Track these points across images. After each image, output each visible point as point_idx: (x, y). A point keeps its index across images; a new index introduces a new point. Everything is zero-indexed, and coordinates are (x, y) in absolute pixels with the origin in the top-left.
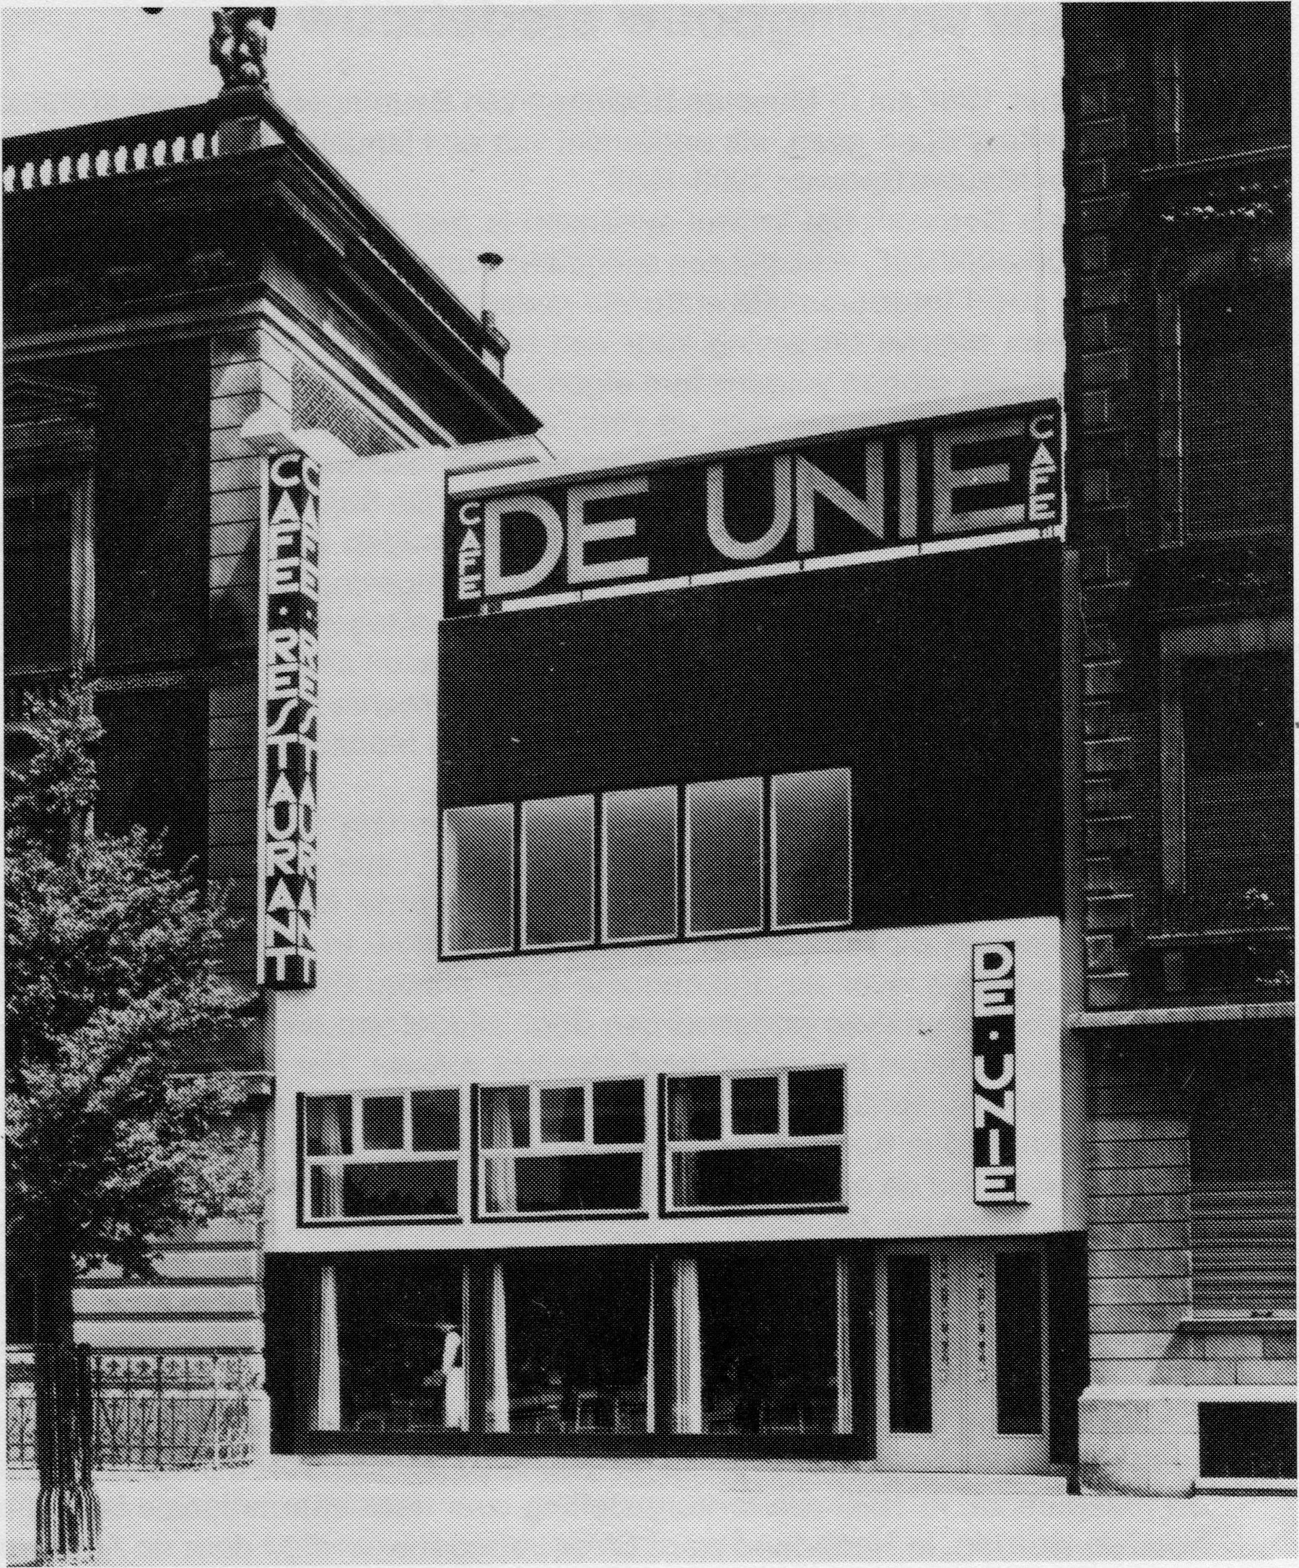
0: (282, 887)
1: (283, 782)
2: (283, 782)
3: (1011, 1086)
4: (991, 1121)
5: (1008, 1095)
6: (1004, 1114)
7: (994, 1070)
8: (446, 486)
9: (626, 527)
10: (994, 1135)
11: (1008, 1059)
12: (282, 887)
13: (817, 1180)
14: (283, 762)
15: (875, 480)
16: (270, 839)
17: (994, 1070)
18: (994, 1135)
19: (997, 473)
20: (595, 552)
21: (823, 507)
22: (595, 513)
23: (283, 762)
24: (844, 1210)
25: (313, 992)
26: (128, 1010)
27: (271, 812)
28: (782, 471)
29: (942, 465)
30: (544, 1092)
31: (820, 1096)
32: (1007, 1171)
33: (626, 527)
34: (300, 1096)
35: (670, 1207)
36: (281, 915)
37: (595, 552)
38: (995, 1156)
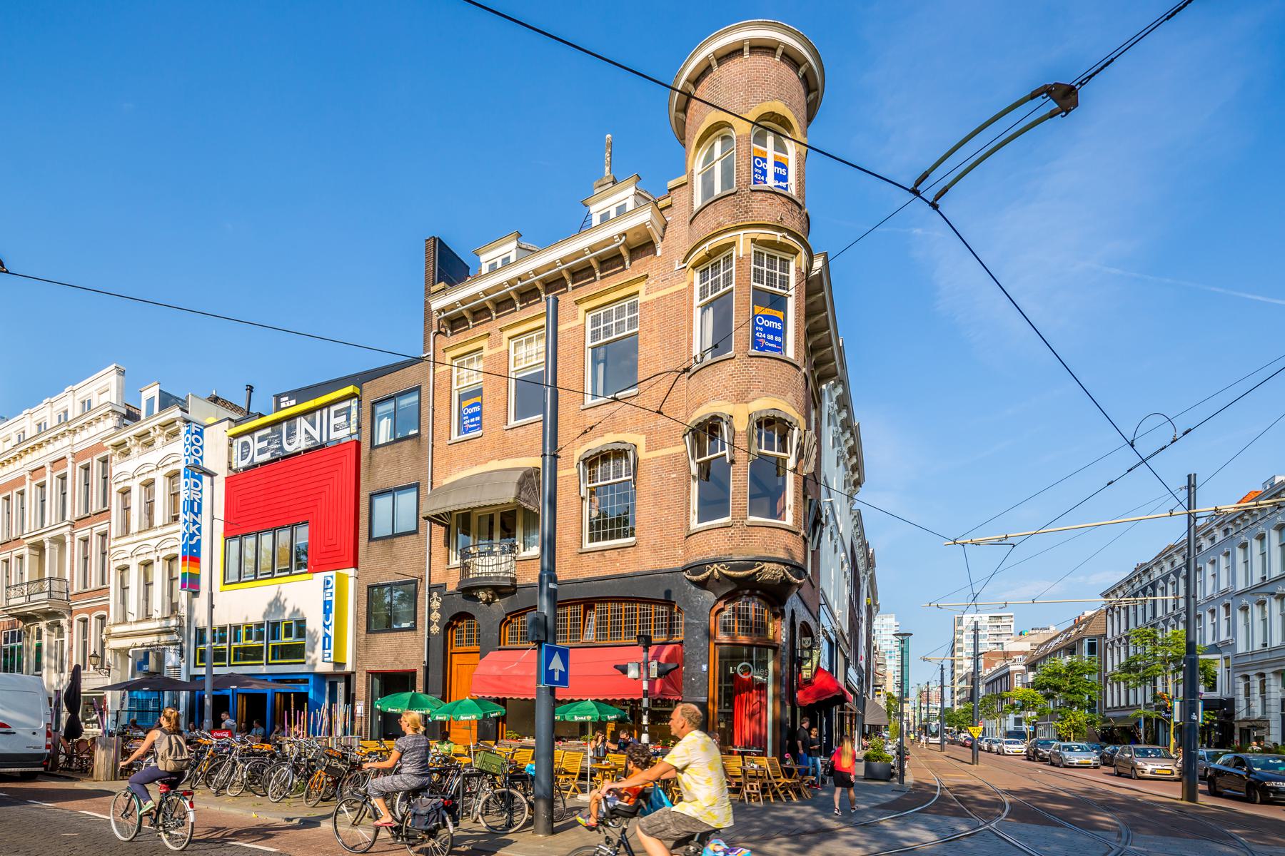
22: (261, 439)
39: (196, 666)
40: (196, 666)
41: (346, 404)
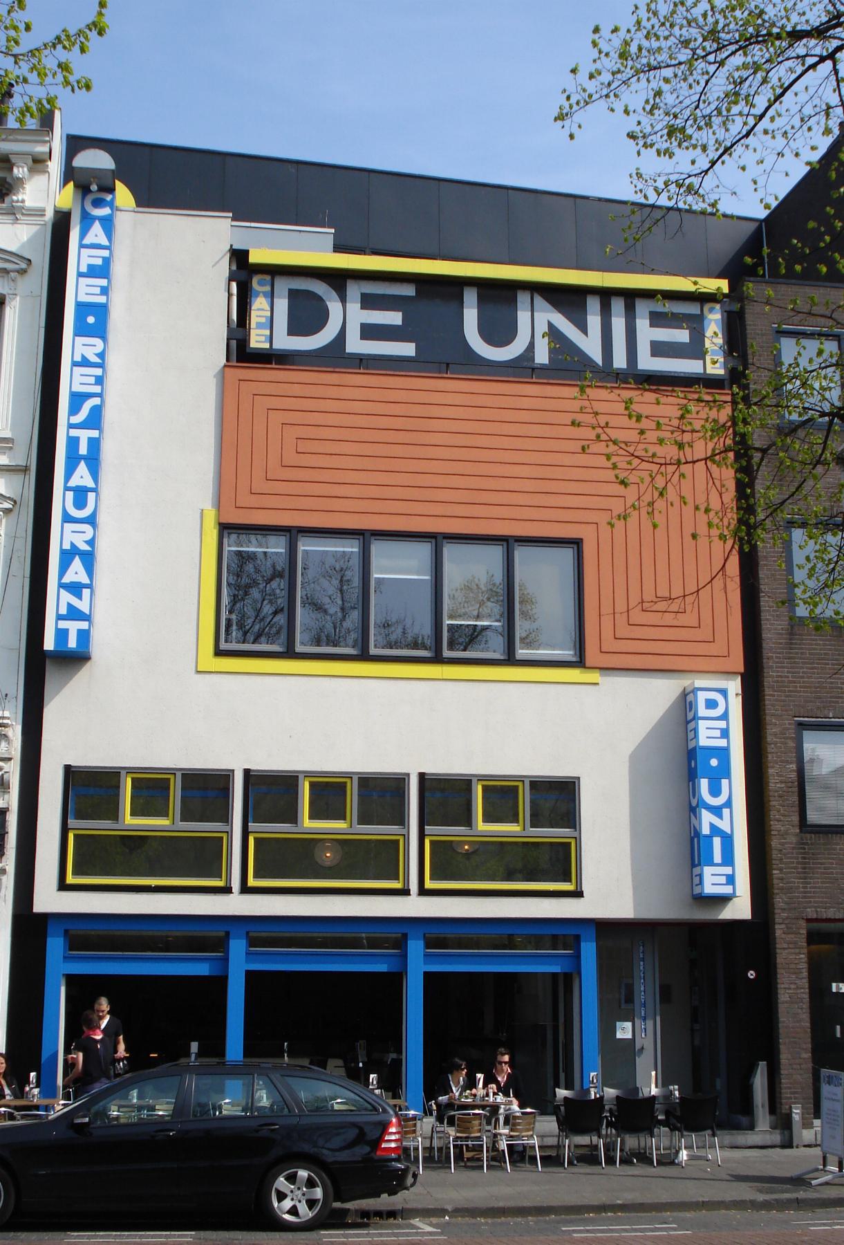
0: (77, 564)
1: (82, 468)
2: (82, 468)
3: (728, 804)
4: (715, 830)
5: (726, 812)
6: (724, 825)
7: (715, 791)
8: (109, 282)
9: (394, 318)
10: (717, 842)
11: (725, 782)
12: (77, 564)
13: (558, 864)
14: (83, 450)
15: (594, 321)
16: (67, 519)
17: (715, 791)
18: (717, 842)
19: (682, 336)
20: (369, 332)
21: (553, 333)
22: (369, 302)
23: (83, 450)
24: (578, 894)
25: (85, 672)
26: (17, 89)
27: (70, 495)
28: (523, 298)
29: (642, 324)
30: (70, 773)
31: (558, 798)
32: (728, 870)
33: (394, 318)
34: (68, 769)
35: (252, 882)
36: (75, 589)
37: (369, 332)
38: (717, 858)
39: (63, 886)
40: (63, 886)
41: (692, 309)
